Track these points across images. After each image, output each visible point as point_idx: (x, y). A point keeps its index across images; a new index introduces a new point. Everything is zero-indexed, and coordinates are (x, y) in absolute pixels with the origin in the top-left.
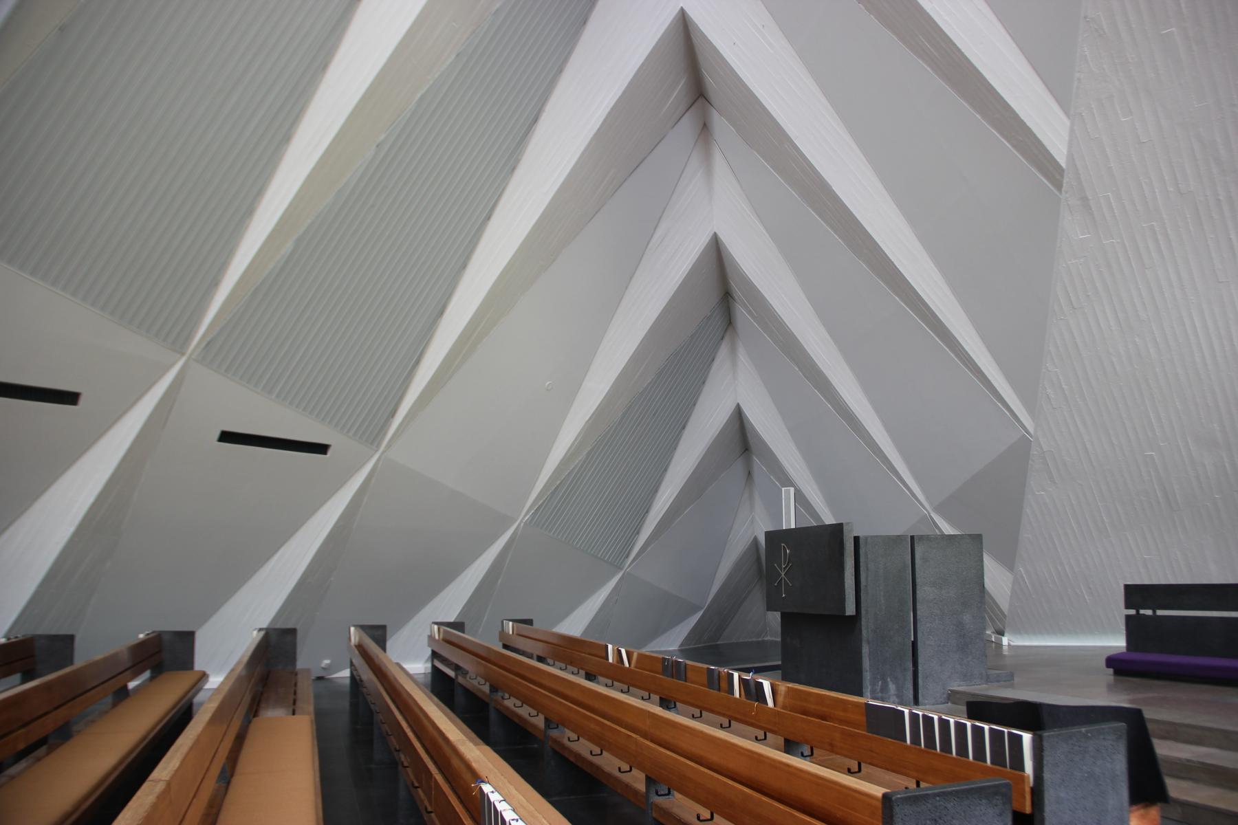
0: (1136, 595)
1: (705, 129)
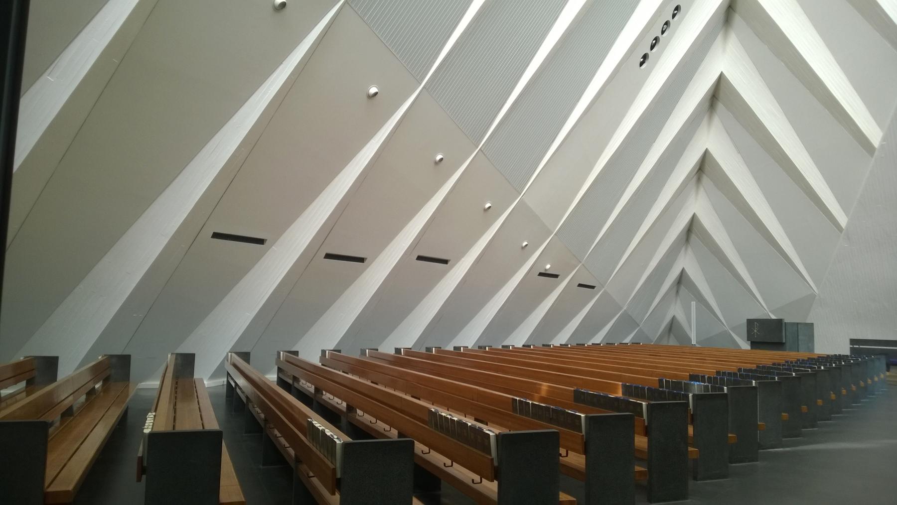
0: (853, 342)
1: (699, 180)
